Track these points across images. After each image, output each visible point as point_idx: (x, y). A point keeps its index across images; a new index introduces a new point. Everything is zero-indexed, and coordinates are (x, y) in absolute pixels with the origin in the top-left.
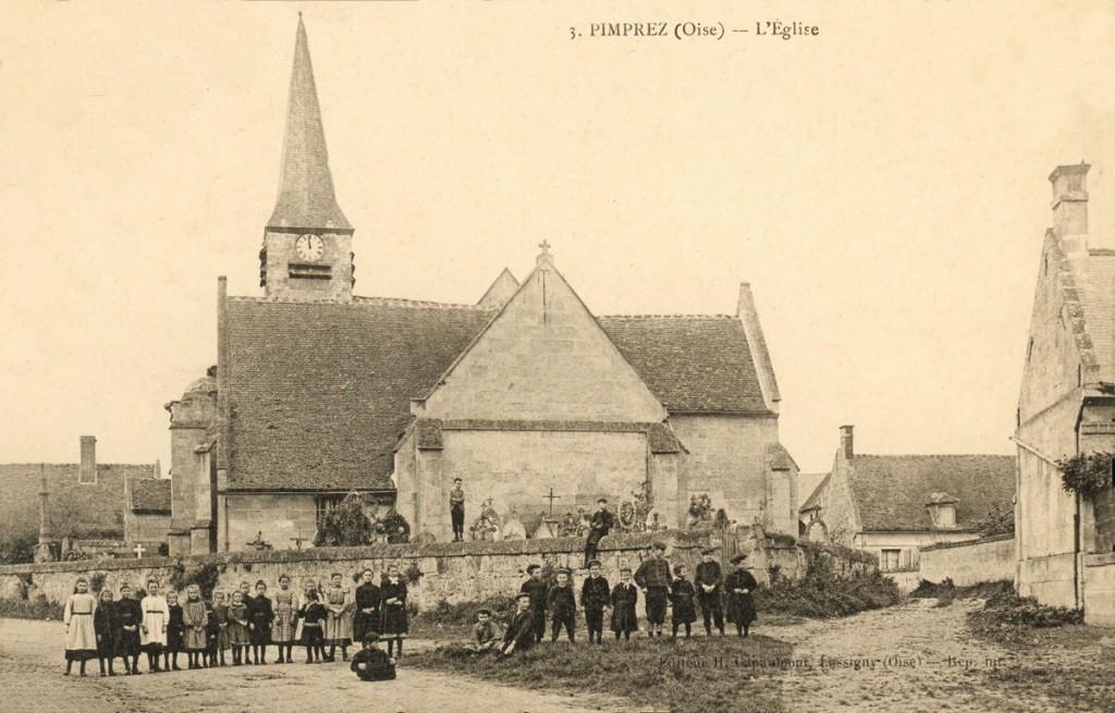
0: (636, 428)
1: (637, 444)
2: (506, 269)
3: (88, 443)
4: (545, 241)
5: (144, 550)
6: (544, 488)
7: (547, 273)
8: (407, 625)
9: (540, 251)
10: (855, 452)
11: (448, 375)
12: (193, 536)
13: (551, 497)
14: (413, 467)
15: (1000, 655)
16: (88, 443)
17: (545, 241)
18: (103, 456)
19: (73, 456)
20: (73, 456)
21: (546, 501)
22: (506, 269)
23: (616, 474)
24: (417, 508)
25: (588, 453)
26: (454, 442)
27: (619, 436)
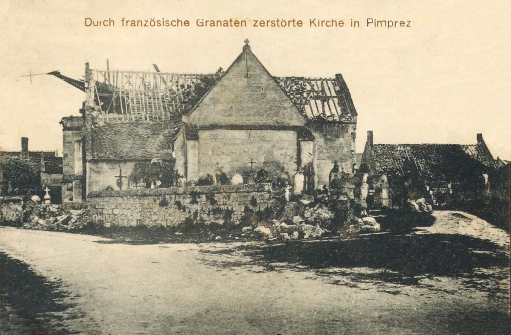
0: (294, 128)
1: (291, 136)
2: (410, 22)
3: (25, 141)
4: (247, 40)
5: (49, 190)
6: (249, 159)
7: (248, 55)
8: (265, 209)
9: (245, 44)
10: (374, 143)
11: (201, 102)
12: (74, 183)
13: (252, 163)
14: (184, 146)
15: (165, 308)
16: (25, 141)
17: (247, 40)
18: (32, 148)
19: (19, 148)
20: (19, 148)
21: (250, 165)
22: (410, 22)
23: (283, 152)
24: (186, 168)
25: (269, 141)
26: (204, 135)
27: (284, 132)
